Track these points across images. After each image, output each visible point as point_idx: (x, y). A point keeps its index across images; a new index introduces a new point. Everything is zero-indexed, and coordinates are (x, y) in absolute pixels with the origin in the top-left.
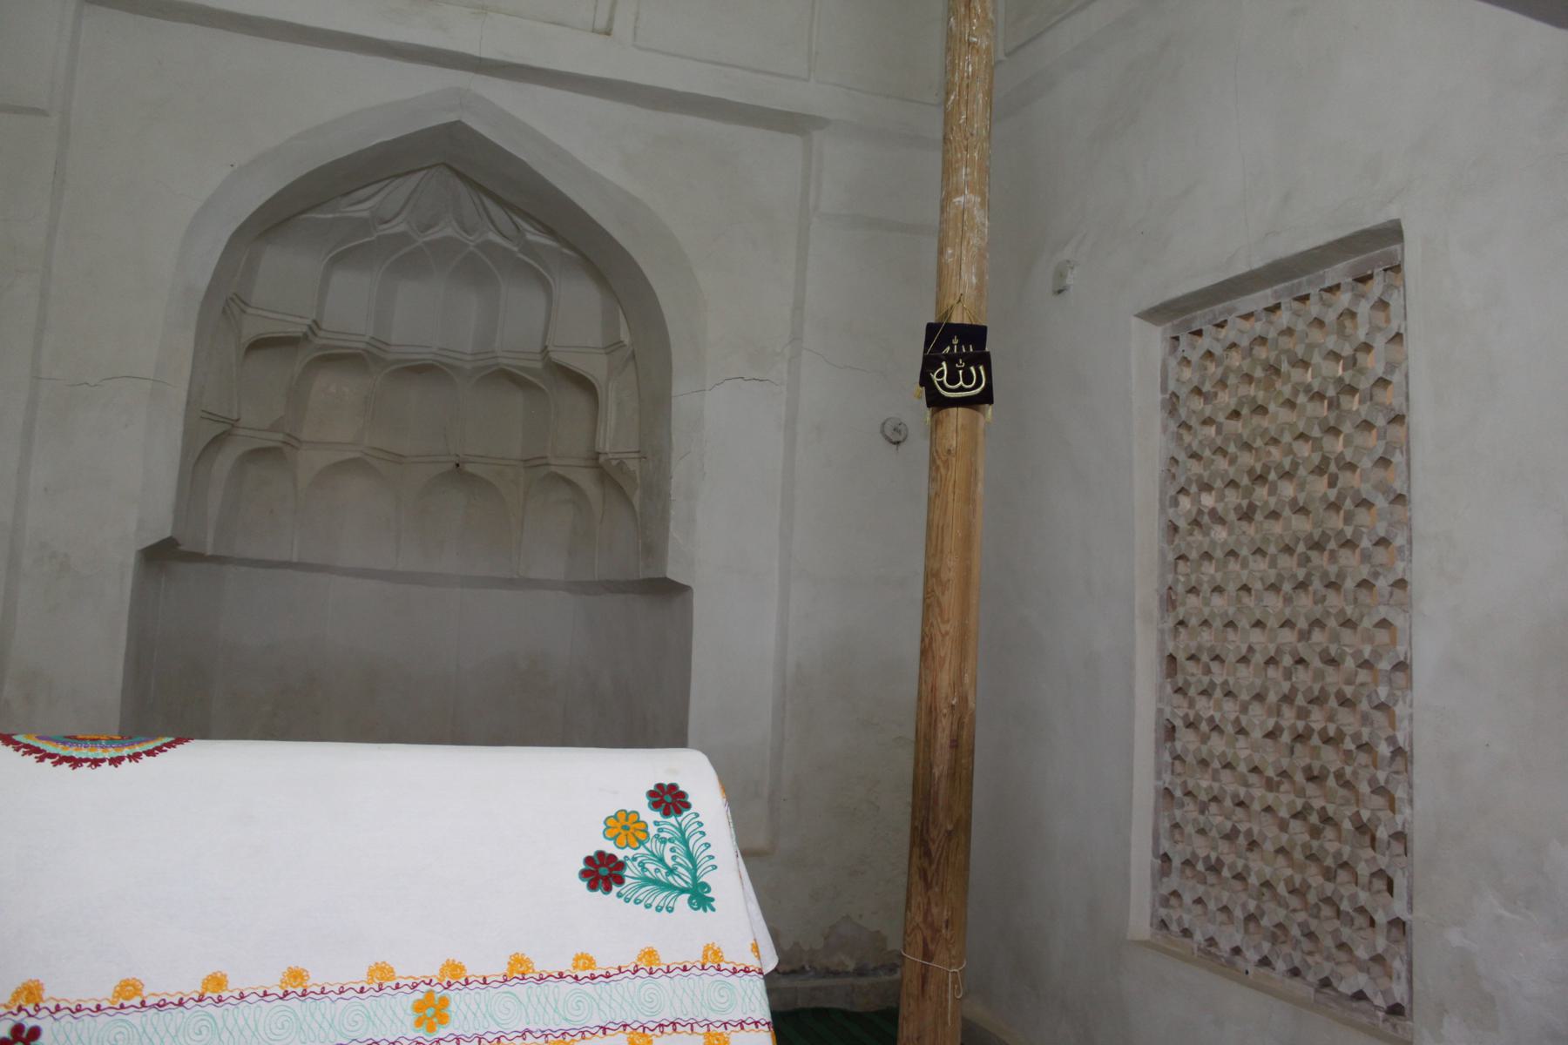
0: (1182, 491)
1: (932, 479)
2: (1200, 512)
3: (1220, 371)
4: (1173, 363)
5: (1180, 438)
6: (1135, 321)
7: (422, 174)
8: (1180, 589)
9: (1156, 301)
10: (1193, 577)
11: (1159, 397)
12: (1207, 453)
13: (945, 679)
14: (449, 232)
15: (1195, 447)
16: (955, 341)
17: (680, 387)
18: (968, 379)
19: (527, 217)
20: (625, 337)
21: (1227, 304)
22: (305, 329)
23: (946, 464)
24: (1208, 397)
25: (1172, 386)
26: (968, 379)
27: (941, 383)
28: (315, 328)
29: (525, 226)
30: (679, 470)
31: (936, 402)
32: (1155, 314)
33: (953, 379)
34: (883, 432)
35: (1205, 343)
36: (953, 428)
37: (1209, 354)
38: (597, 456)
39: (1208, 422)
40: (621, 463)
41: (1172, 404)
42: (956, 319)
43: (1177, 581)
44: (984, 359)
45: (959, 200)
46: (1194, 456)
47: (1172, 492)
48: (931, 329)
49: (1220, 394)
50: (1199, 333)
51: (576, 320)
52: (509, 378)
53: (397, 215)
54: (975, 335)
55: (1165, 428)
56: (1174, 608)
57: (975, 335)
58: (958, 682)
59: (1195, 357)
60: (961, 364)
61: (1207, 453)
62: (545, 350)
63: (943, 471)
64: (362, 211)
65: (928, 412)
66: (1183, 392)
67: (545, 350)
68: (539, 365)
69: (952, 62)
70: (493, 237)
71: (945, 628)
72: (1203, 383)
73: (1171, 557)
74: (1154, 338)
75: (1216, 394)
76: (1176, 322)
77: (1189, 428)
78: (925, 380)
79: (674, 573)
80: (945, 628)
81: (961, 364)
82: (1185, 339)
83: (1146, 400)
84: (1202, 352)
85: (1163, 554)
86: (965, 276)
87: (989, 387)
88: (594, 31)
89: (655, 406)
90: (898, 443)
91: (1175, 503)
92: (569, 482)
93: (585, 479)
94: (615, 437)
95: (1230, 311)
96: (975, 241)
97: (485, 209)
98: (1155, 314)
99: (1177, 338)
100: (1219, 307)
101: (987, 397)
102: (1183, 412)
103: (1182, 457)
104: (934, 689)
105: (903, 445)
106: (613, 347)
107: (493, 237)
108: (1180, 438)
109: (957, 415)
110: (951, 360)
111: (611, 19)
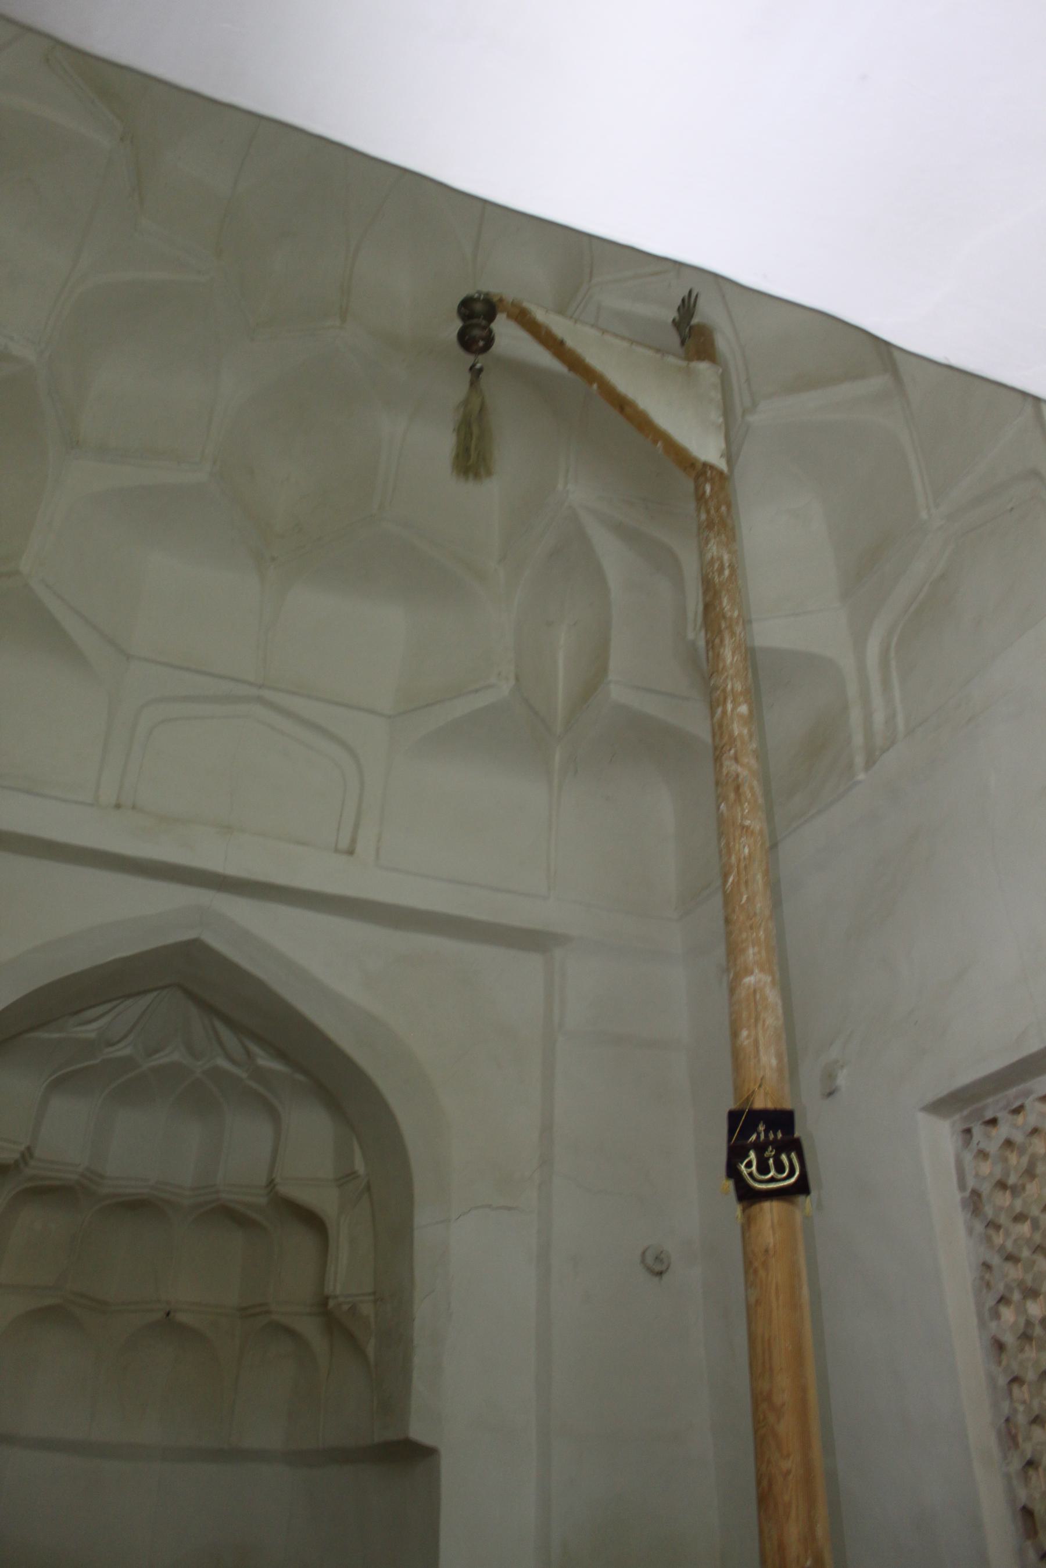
0: (1003, 1300)
1: (749, 1284)
2: (1029, 1323)
3: (1025, 1160)
4: (968, 1157)
5: (989, 1239)
6: (922, 1117)
7: (155, 994)
8: (1021, 1419)
9: (943, 1090)
10: (1036, 1404)
11: (958, 1196)
12: (1026, 1253)
13: (793, 1532)
14: (176, 1057)
15: (1009, 1246)
16: (761, 1128)
17: (423, 1217)
18: (780, 1168)
19: (260, 1040)
20: (360, 1166)
21: (1021, 1087)
22: (17, 1156)
23: (765, 1264)
24: (1015, 1191)
25: (971, 1183)
26: (780, 1168)
27: (751, 1174)
28: (28, 1154)
29: (254, 1048)
30: (422, 1310)
31: (747, 1195)
32: (941, 1106)
33: (763, 1169)
34: (643, 1260)
35: (1003, 1131)
36: (769, 1224)
37: (1008, 1143)
38: (324, 1301)
39: (1019, 1218)
40: (353, 1309)
41: (974, 1202)
42: (759, 1104)
43: (1015, 1411)
44: (794, 1145)
45: (749, 980)
46: (1011, 1258)
47: (990, 1302)
48: (733, 1117)
49: (1028, 1187)
50: (993, 1122)
51: (307, 1150)
52: (229, 1215)
53: (125, 1036)
54: (782, 1120)
55: (970, 1231)
56: (1016, 1445)
57: (782, 1120)
58: (809, 1537)
59: (993, 1147)
60: (770, 1152)
61: (1026, 1253)
62: (271, 1183)
63: (762, 1273)
64: (89, 1032)
65: (738, 1209)
66: (986, 1188)
67: (271, 1183)
68: (263, 1201)
69: (728, 844)
70: (222, 1062)
71: (786, 1465)
72: (1008, 1175)
73: (1002, 1381)
74: (940, 1136)
75: (1023, 1187)
76: (965, 1113)
77: (998, 1227)
78: (732, 1172)
79: (419, 1432)
80: (786, 1465)
81: (770, 1152)
82: (978, 1130)
83: (944, 1199)
84: (1001, 1141)
85: (992, 1380)
86: (764, 1059)
87: (804, 1176)
88: (337, 850)
89: (394, 1235)
90: (660, 1274)
91: (996, 1315)
92: (290, 1332)
93: (309, 1328)
94: (348, 1276)
95: (1027, 1094)
96: (770, 1021)
97: (216, 1033)
98: (941, 1106)
99: (968, 1131)
100: (1013, 1091)
101: (802, 1187)
102: (989, 1211)
103: (996, 1261)
104: (781, 1547)
105: (665, 1277)
106: (345, 1178)
107: (222, 1062)
108: (989, 1239)
109: (770, 1209)
110: (760, 1148)
111: (353, 841)
